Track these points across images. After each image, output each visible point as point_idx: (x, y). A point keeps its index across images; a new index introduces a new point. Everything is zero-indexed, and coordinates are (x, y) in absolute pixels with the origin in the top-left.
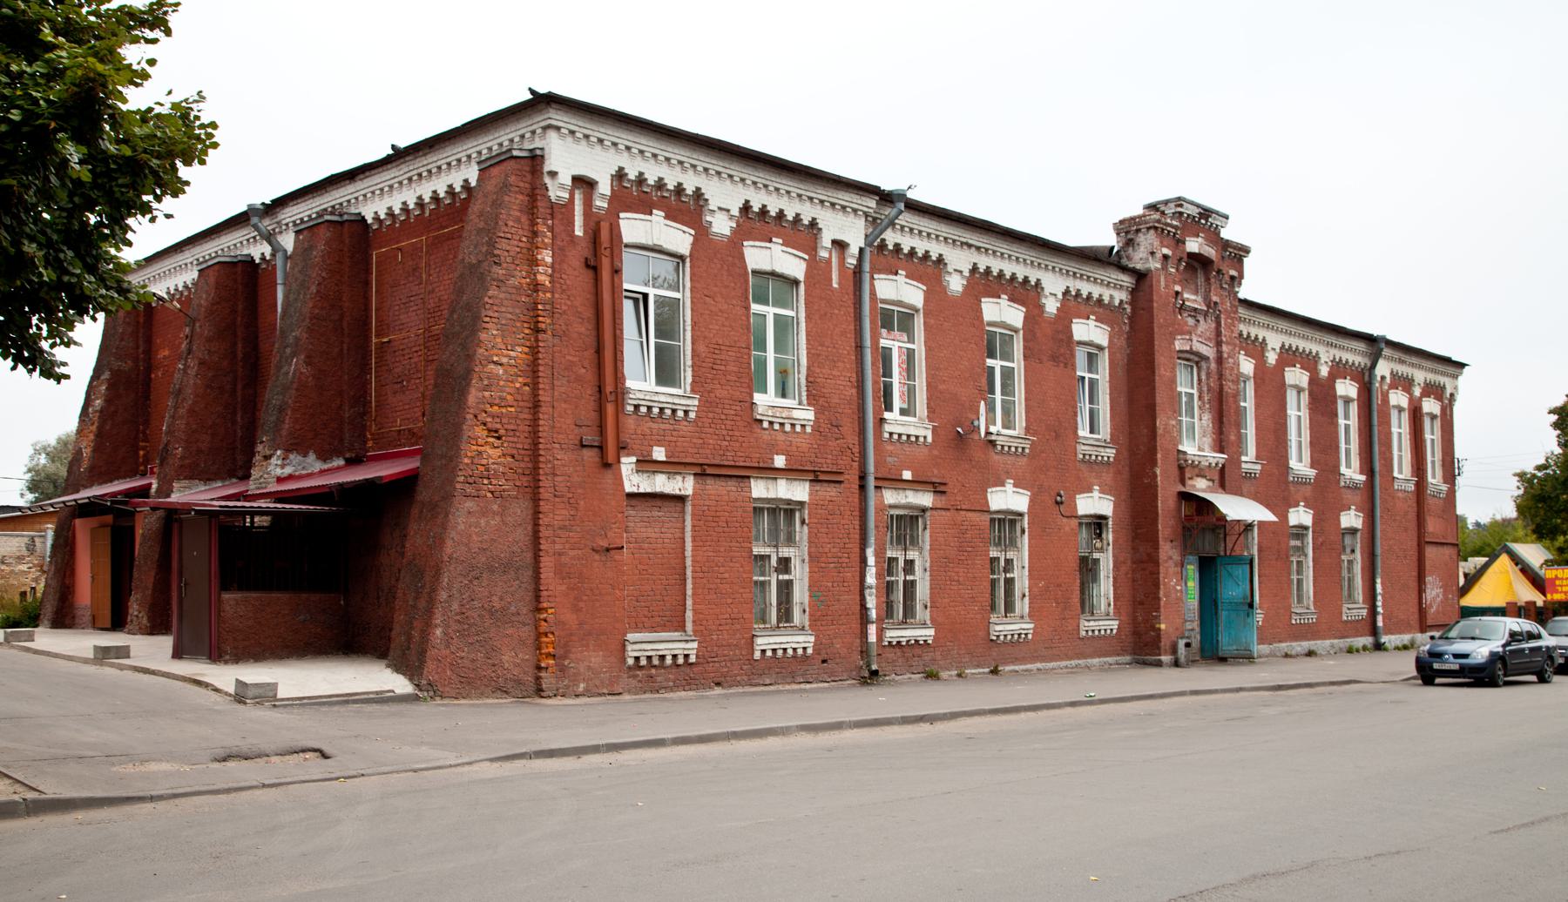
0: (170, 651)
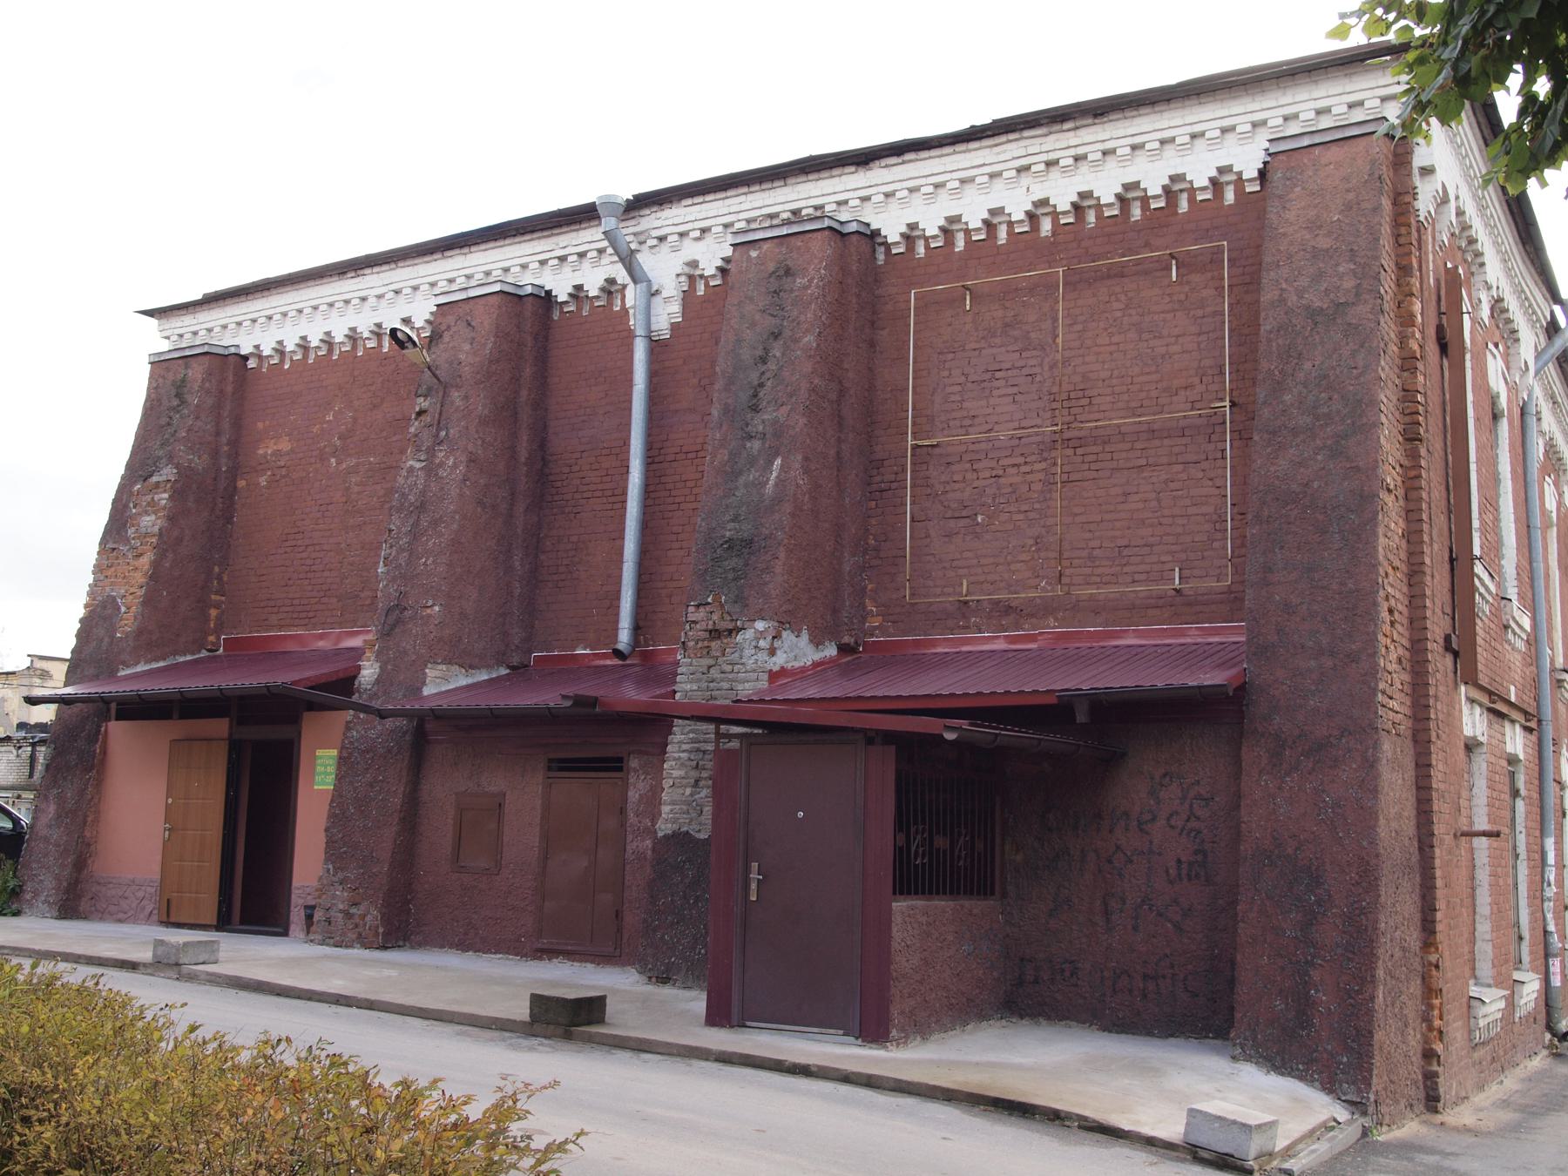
0: (608, 1001)
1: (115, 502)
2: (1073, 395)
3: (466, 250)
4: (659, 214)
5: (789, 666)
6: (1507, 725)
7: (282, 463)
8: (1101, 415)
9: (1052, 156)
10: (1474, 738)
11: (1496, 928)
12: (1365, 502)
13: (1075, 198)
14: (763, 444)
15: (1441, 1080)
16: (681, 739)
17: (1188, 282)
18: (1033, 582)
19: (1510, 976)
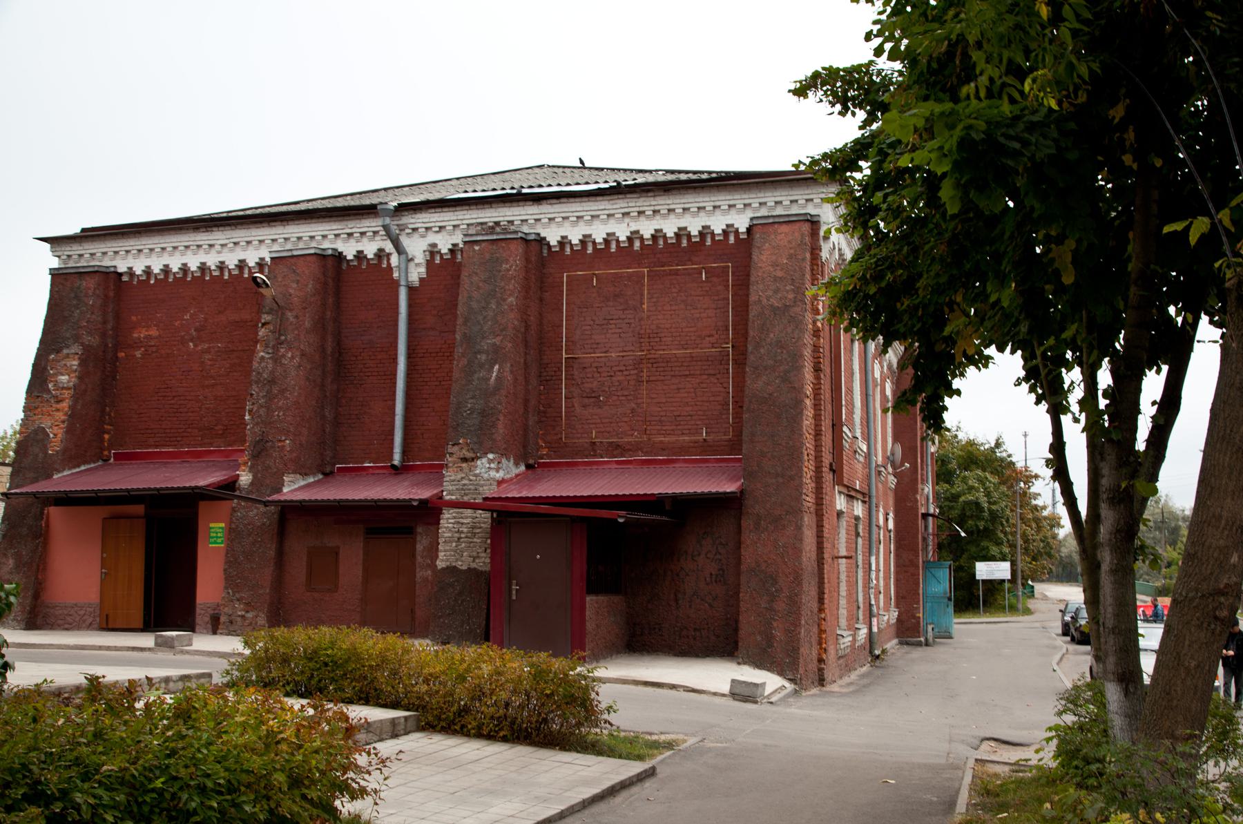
1: (34, 366)
2: (651, 336)
3: (285, 223)
4: (413, 216)
5: (505, 477)
6: (855, 502)
7: (153, 344)
8: (665, 347)
9: (641, 209)
10: (841, 510)
11: (848, 602)
12: (798, 404)
13: (653, 232)
14: (488, 356)
15: (825, 672)
16: (448, 519)
17: (711, 282)
18: (630, 433)
19: (854, 626)
